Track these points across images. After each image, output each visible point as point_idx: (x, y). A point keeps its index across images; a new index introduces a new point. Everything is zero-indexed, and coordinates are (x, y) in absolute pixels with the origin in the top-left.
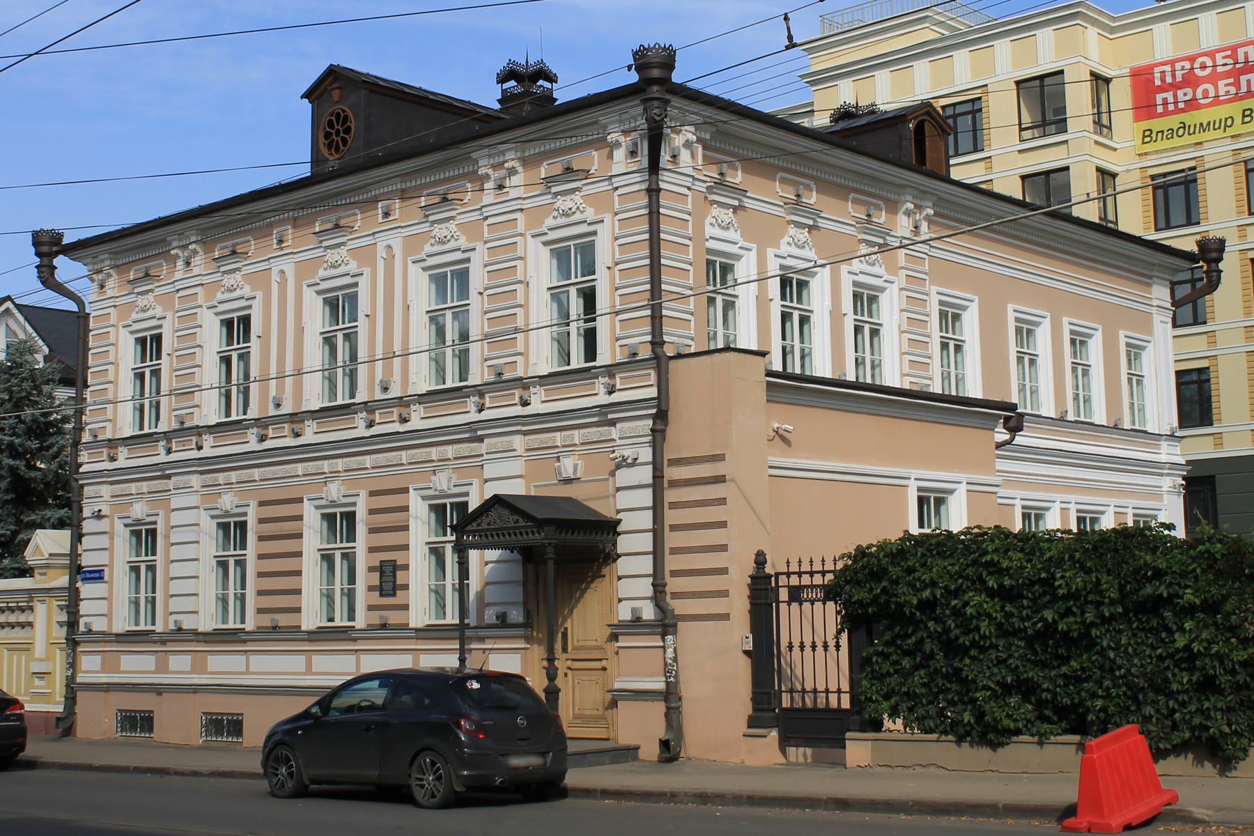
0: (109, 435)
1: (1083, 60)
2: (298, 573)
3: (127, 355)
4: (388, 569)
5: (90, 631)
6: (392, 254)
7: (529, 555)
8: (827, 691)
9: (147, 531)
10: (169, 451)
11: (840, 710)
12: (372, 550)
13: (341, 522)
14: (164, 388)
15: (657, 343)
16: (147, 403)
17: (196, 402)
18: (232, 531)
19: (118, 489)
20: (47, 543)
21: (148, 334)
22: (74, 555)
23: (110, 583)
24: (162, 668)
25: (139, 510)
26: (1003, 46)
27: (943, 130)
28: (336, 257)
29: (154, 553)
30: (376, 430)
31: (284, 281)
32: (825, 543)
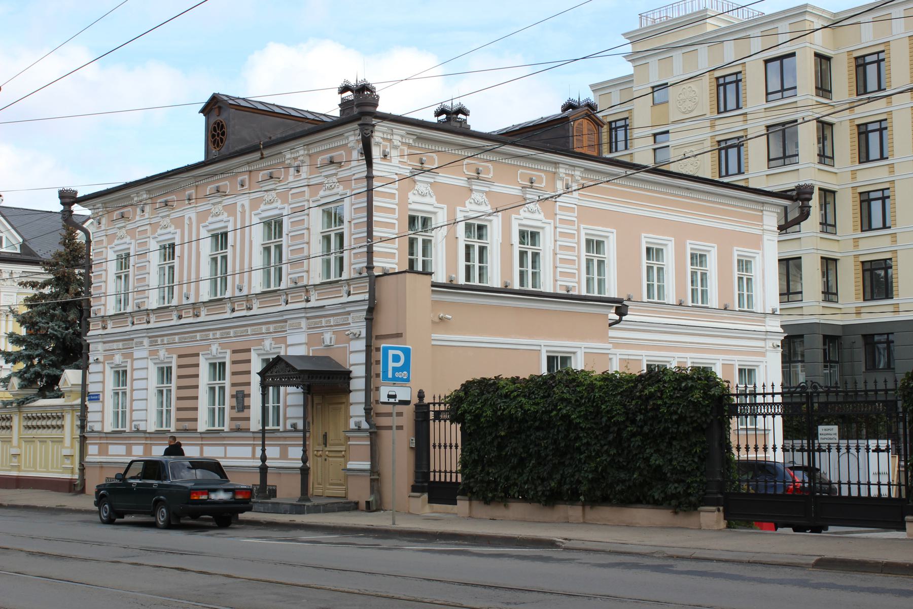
0: (102, 314)
1: (809, 45)
2: (196, 398)
3: (112, 268)
4: (240, 396)
5: (93, 431)
6: (244, 207)
7: (309, 392)
8: (849, 483)
9: (220, 363)
10: (133, 324)
11: (457, 483)
12: (233, 385)
13: (218, 369)
14: (284, 260)
15: (370, 268)
16: (332, 257)
17: (146, 295)
18: (165, 373)
19: (108, 346)
20: (71, 377)
21: (219, 231)
22: (84, 385)
23: (103, 402)
24: (129, 453)
25: (118, 359)
26: (703, 50)
27: (598, 125)
28: (217, 210)
29: (224, 379)
30: (183, 321)
31: (190, 224)
32: (441, 385)
